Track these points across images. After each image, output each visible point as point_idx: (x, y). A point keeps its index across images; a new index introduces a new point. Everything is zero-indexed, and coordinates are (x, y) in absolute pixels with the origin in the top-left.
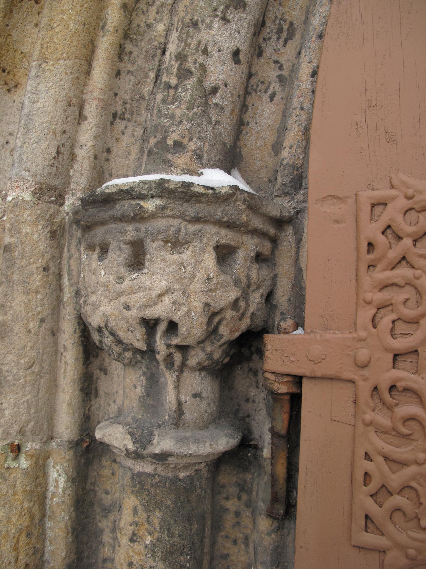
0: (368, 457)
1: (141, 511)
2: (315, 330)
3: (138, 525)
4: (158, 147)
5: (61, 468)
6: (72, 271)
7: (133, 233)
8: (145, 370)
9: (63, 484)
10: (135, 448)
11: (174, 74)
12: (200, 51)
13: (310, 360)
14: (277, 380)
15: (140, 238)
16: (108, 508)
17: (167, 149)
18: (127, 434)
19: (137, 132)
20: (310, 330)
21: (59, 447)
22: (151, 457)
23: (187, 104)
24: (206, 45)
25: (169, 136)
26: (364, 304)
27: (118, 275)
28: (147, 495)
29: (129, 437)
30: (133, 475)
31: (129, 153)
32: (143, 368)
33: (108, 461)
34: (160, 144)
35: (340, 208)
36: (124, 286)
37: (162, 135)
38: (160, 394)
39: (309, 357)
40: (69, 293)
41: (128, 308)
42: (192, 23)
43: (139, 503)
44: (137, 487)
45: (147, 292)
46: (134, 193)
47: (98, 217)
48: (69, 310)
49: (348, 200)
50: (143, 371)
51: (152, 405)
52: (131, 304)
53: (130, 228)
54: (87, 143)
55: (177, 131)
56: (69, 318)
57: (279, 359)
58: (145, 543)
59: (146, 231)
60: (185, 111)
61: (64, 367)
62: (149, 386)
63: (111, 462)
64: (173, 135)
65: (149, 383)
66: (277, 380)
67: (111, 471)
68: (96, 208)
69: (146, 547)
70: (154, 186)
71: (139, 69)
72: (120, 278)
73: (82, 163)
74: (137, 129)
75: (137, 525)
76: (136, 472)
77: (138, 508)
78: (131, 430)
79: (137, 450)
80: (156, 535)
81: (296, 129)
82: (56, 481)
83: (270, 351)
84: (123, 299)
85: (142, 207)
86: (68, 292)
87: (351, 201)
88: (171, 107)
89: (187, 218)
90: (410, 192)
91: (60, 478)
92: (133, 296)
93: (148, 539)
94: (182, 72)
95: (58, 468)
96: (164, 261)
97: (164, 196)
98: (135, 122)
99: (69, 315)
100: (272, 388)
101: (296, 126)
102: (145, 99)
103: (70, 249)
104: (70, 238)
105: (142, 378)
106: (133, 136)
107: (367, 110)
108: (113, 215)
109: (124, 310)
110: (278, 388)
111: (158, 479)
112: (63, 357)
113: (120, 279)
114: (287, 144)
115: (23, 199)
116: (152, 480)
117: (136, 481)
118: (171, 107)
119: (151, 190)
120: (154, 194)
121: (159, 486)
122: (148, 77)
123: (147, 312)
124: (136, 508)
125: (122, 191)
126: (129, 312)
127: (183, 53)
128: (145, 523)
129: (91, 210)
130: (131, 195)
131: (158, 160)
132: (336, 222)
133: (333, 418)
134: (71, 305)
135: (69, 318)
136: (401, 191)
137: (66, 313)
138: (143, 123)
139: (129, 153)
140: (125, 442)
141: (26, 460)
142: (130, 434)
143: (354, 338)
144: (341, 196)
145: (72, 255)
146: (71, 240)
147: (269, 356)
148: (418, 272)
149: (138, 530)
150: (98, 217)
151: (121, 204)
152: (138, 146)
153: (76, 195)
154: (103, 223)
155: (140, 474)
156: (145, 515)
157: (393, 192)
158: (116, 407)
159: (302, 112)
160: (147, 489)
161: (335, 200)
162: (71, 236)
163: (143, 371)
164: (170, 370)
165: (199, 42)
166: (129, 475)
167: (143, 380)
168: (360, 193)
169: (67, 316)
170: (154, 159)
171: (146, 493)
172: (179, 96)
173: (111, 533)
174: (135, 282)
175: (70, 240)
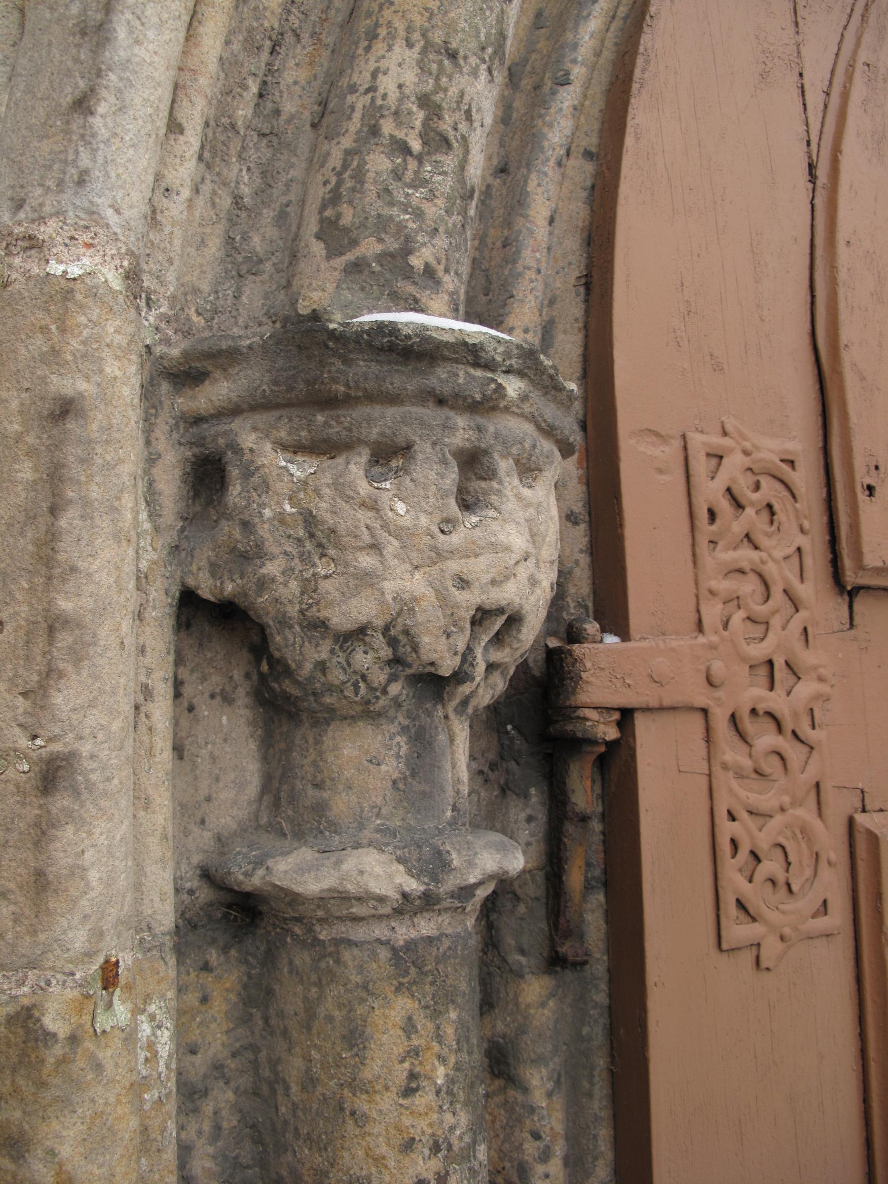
0: (732, 817)
1: (424, 1021)
2: (645, 636)
3: (421, 1053)
4: (384, 263)
5: (161, 1008)
6: (160, 494)
7: (471, 434)
8: (406, 722)
9: (167, 1048)
10: (425, 887)
11: (417, 131)
12: (462, 112)
13: (655, 682)
14: (602, 720)
15: (483, 446)
16: (200, 1086)
17: (408, 273)
18: (395, 863)
19: (220, 198)
20: (639, 636)
21: (149, 955)
22: (452, 897)
23: (445, 200)
24: (470, 105)
25: (419, 251)
26: (710, 596)
27: (445, 515)
28: (432, 983)
29: (401, 868)
30: (394, 950)
31: (203, 241)
32: (401, 718)
33: (191, 970)
34: (389, 259)
35: (663, 451)
36: (456, 539)
37: (399, 241)
38: (436, 769)
39: (654, 676)
40: (154, 549)
41: (463, 583)
42: (447, 50)
43: (417, 1005)
44: (409, 973)
45: (500, 555)
46: (483, 354)
47: (392, 384)
48: (154, 593)
49: (672, 441)
50: (400, 724)
51: (423, 794)
52: (472, 577)
53: (461, 421)
54: (180, 189)
55: (429, 245)
56: (154, 614)
57: (609, 684)
58: (436, 1083)
59: (497, 436)
60: (443, 212)
61: (148, 741)
62: (416, 755)
63: (196, 973)
64: (424, 250)
65: (415, 749)
66: (602, 720)
67: (199, 995)
68: (377, 361)
69: (438, 1093)
70: (515, 352)
71: (233, 62)
72: (447, 521)
73: (172, 233)
74: (220, 192)
75: (417, 1054)
76: (401, 943)
77: (415, 1017)
78: (399, 852)
79: (430, 889)
80: (452, 1060)
81: (533, 303)
82: (151, 1046)
83: (591, 672)
84: (453, 566)
85: (500, 386)
86: (150, 548)
87: (677, 444)
88: (414, 194)
89: (543, 425)
90: (747, 445)
91: (159, 1033)
92: (473, 560)
93: (441, 1074)
94: (432, 134)
95: (152, 1008)
96: (519, 497)
97: (526, 375)
98: (218, 174)
99: (154, 608)
100: (597, 733)
101: (531, 297)
102: (238, 133)
103: (152, 439)
104: (153, 411)
105: (398, 739)
106: (214, 205)
107: (686, 316)
108: (433, 388)
109: (454, 589)
110: (604, 733)
111: (446, 943)
112: (142, 716)
113: (447, 525)
114: (519, 323)
115: (106, 281)
116: (438, 949)
117: (406, 962)
118: (414, 194)
119: (510, 358)
120: (515, 366)
121: (449, 957)
122: (245, 88)
123: (492, 595)
124: (410, 1019)
125: (465, 344)
126: (463, 593)
127: (434, 98)
128: (434, 1043)
129: (361, 363)
130: (477, 357)
131: (375, 287)
132: (660, 471)
133: (681, 769)
134: (158, 583)
135: (154, 614)
136: (737, 443)
137: (147, 601)
138: (233, 185)
139: (203, 241)
140: (398, 880)
141: (124, 1002)
142: (399, 860)
143: (703, 646)
144: (663, 433)
145: (160, 456)
146: (156, 416)
147: (589, 680)
148: (764, 555)
149: (421, 1063)
150: (392, 384)
151: (449, 369)
152: (220, 229)
153: (159, 307)
154: (393, 399)
155: (410, 946)
156: (430, 1026)
157: (726, 442)
158: (207, 835)
159: (539, 277)
160: (430, 971)
161: (654, 439)
162: (154, 407)
163: (400, 724)
164: (461, 716)
165: (462, 94)
166: (384, 954)
167: (402, 744)
168: (690, 435)
169: (149, 609)
170: (364, 284)
171: (430, 978)
172: (427, 178)
173: (211, 1145)
174: (478, 532)
175: (151, 415)
